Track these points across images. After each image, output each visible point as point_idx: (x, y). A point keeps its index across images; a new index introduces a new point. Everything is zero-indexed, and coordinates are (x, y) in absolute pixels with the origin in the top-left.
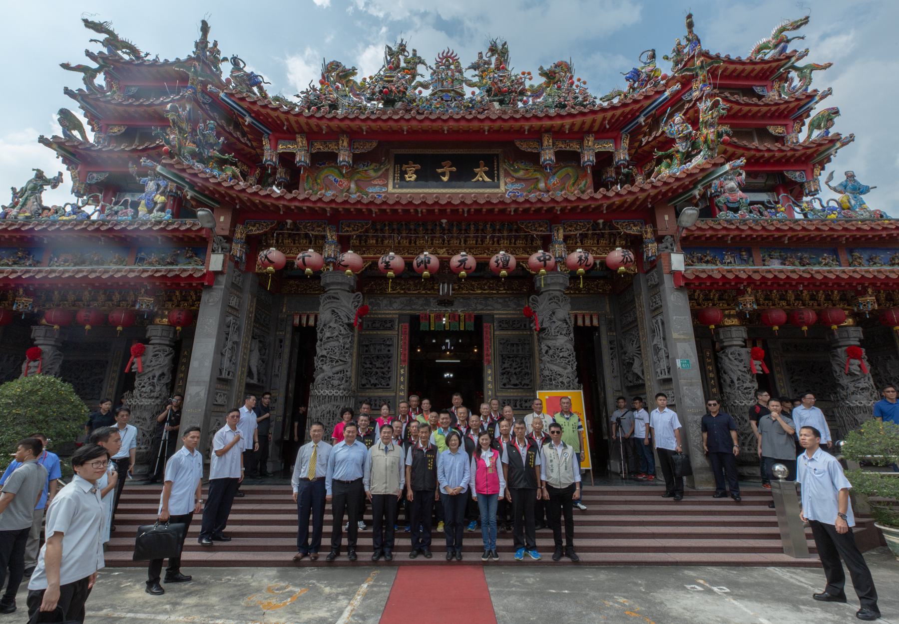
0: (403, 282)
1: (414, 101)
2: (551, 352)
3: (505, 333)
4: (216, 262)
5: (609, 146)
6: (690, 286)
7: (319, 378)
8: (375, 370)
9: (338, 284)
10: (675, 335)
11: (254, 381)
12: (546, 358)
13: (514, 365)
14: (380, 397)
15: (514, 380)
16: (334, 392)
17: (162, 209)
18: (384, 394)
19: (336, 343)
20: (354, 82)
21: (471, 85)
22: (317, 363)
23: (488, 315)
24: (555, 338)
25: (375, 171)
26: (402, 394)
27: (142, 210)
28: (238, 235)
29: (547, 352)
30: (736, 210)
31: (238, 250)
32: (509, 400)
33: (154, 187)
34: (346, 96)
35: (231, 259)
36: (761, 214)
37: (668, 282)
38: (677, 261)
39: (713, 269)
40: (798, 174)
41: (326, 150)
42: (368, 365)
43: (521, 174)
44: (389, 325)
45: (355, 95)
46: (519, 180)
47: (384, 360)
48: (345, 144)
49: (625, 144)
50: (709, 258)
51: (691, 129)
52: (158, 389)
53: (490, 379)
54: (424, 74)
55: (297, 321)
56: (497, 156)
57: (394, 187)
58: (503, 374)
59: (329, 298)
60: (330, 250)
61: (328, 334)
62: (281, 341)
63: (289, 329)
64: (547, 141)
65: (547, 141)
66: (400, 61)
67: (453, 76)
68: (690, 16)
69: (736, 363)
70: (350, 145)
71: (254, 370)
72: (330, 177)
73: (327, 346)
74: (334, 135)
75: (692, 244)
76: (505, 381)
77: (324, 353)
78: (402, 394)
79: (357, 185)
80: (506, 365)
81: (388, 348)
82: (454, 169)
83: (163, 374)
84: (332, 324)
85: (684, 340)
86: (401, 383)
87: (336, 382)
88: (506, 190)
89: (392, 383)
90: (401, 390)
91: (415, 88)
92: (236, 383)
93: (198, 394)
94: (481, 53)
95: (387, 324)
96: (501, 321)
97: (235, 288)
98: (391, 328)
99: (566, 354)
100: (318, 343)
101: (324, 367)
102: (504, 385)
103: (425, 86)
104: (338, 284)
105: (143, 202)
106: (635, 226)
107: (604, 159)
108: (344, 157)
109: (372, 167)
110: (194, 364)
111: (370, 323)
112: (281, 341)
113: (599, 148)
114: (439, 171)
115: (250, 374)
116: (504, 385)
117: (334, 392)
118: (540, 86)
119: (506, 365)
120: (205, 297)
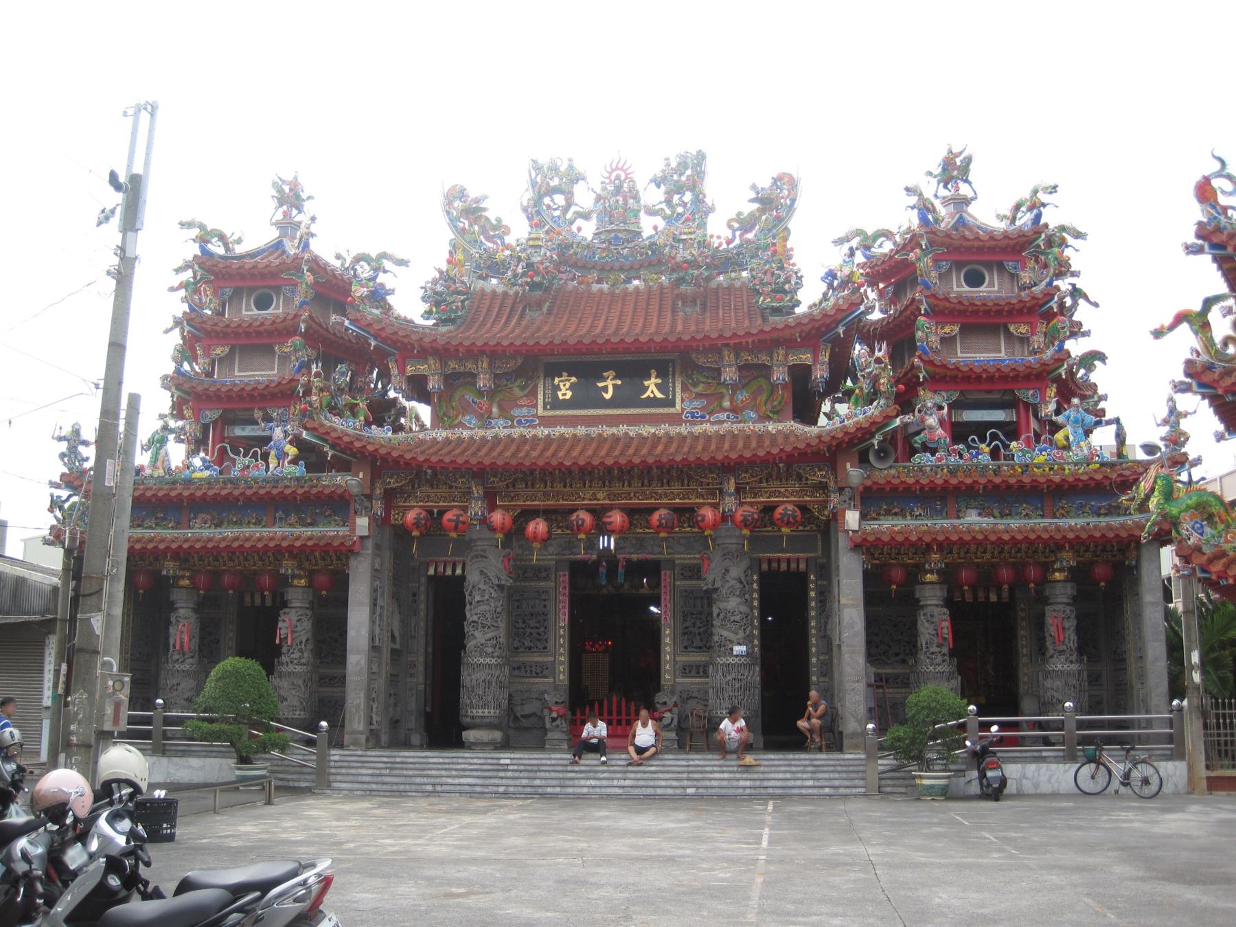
0: (559, 518)
1: (572, 246)
2: (722, 616)
3: (688, 583)
4: (362, 523)
5: (806, 358)
6: (861, 545)
7: (470, 644)
8: (529, 630)
9: (485, 539)
10: (843, 601)
11: (397, 646)
12: (716, 623)
13: (698, 624)
14: (536, 663)
15: (697, 643)
16: (488, 660)
17: (294, 462)
18: (541, 659)
19: (486, 608)
20: (487, 219)
21: (652, 212)
22: (467, 628)
23: (667, 560)
24: (726, 600)
25: (522, 388)
26: (562, 659)
27: (273, 462)
28: (378, 491)
29: (718, 615)
30: (933, 452)
31: (378, 507)
32: (698, 667)
33: (282, 435)
34: (476, 241)
35: (374, 520)
36: (961, 456)
37: (843, 543)
38: (852, 518)
39: (888, 525)
40: (1031, 392)
41: (462, 369)
42: (521, 625)
43: (700, 389)
44: (544, 574)
45: (488, 239)
46: (699, 396)
47: (540, 618)
48: (485, 365)
49: (825, 357)
50: (897, 510)
51: (921, 319)
52: (306, 655)
53: (668, 640)
54: (584, 198)
55: (431, 572)
56: (673, 361)
57: (545, 408)
58: (684, 634)
59: (477, 556)
60: (477, 508)
61: (478, 598)
62: (414, 595)
63: (423, 580)
64: (728, 356)
65: (728, 356)
66: (550, 185)
67: (626, 203)
68: (907, 189)
69: (927, 625)
70: (490, 365)
71: (397, 634)
72: (467, 397)
73: (478, 610)
74: (474, 353)
75: (873, 499)
76: (686, 643)
77: (475, 618)
78: (562, 659)
79: (501, 408)
80: (688, 624)
81: (543, 603)
82: (619, 382)
83: (307, 640)
84: (482, 587)
85: (852, 606)
86: (561, 646)
87: (489, 650)
88: (683, 410)
89: (550, 645)
90: (561, 655)
91: (571, 223)
92: (384, 650)
93: (358, 663)
94: (667, 159)
95: (540, 572)
96: (684, 567)
97: (377, 547)
98: (547, 578)
99: (737, 618)
100: (468, 607)
101: (476, 634)
102: (686, 648)
103: (586, 216)
104: (485, 539)
105: (272, 453)
106: (820, 470)
107: (800, 374)
108: (483, 382)
109: (518, 383)
110: (351, 633)
111: (520, 572)
112: (414, 595)
113: (793, 360)
114: (600, 385)
115: (393, 638)
116: (686, 648)
117: (488, 660)
118: (751, 214)
119: (688, 624)
120: (353, 563)
